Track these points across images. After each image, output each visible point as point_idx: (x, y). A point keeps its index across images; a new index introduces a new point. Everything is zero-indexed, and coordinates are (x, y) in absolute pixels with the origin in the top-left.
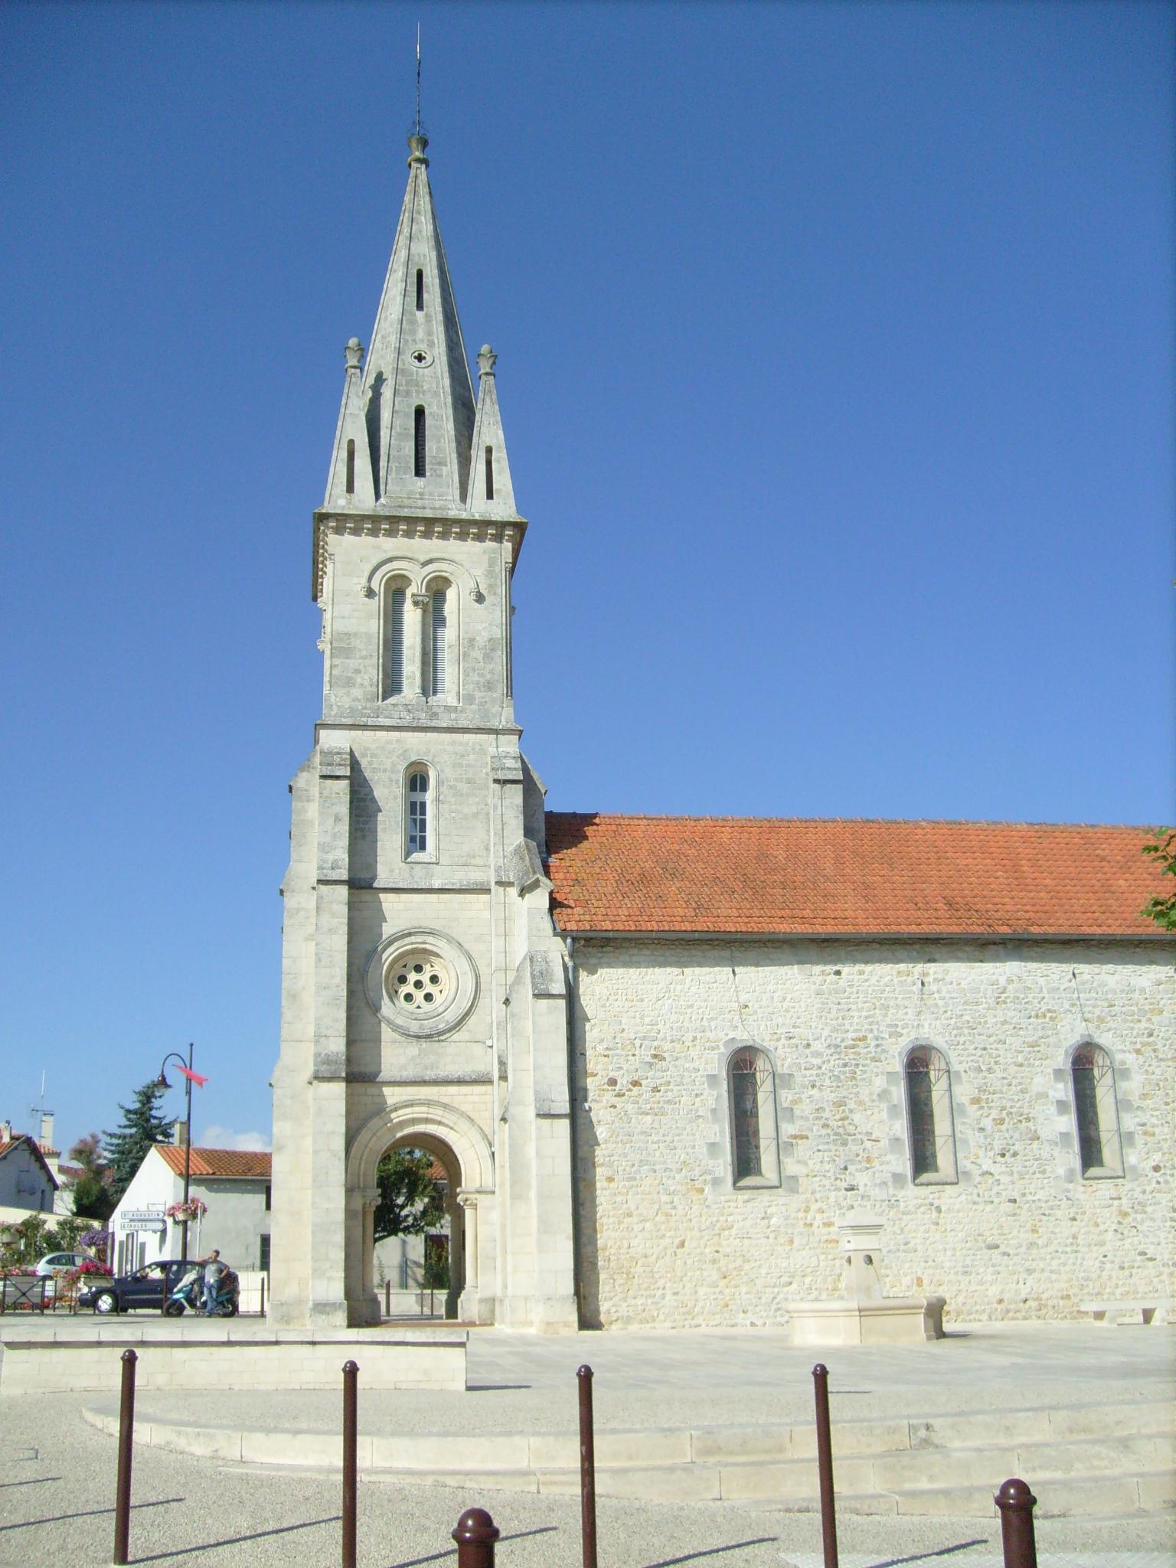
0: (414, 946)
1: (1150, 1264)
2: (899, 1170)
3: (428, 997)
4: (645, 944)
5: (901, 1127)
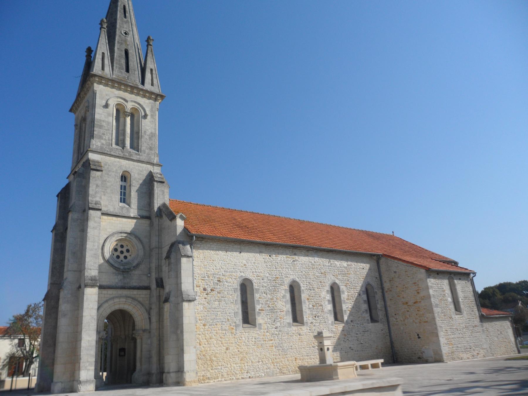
1: (352, 351)
2: (288, 321)
3: (125, 257)
5: (289, 307)
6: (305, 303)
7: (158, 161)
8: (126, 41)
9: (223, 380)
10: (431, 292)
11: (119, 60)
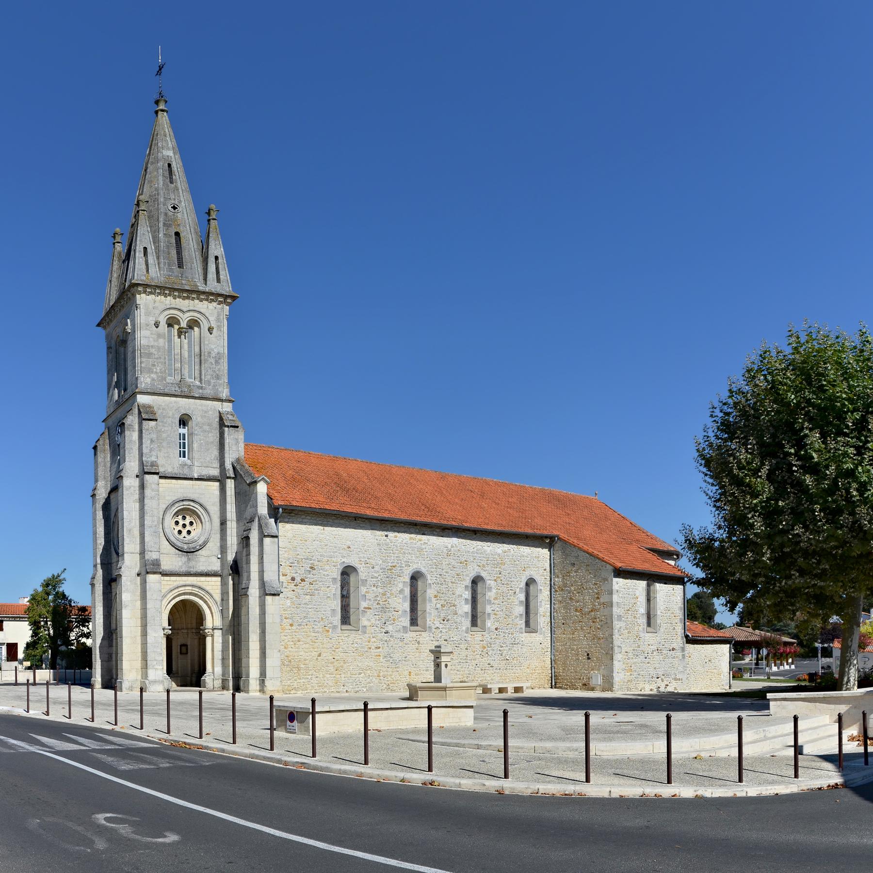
0: (184, 507)
1: (491, 668)
2: (404, 625)
3: (189, 532)
4: (308, 513)
5: (407, 606)
6: (430, 601)
7: (229, 394)
8: (175, 220)
9: (313, 691)
10: (615, 599)
11: (168, 252)
